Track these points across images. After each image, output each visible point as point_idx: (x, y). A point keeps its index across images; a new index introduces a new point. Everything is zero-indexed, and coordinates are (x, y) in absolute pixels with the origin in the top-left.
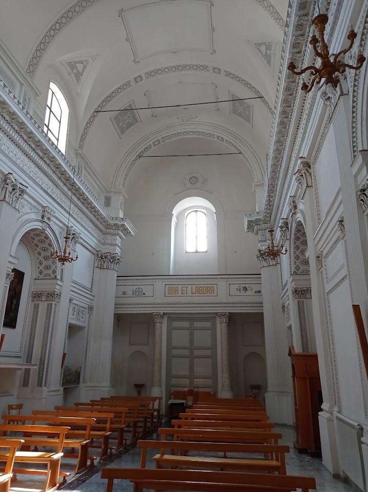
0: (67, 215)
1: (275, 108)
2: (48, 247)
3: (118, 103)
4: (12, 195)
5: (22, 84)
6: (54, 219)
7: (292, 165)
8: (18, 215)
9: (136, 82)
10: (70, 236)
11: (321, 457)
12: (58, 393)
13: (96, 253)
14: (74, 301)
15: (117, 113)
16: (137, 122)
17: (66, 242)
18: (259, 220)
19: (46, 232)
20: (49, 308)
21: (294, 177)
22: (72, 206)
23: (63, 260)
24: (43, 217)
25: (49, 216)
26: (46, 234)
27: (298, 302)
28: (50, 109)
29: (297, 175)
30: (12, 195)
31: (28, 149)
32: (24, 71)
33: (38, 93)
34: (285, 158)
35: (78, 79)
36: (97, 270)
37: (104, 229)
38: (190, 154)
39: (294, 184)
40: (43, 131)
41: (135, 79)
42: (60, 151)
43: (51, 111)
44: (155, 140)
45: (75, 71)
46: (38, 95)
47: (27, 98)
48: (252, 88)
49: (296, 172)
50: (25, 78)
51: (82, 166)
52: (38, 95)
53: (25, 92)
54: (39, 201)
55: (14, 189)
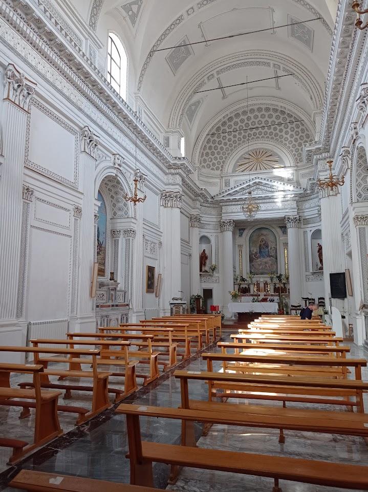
0: (134, 161)
1: (335, 28)
2: (116, 184)
3: (173, 40)
4: (90, 146)
5: (86, 39)
6: (123, 165)
7: (353, 91)
8: (97, 163)
9: (189, 15)
10: (139, 178)
11: (289, 297)
12: (140, 314)
13: (189, 216)
14: (146, 237)
15: (172, 51)
16: (190, 54)
17: (136, 184)
18: (319, 149)
19: (118, 178)
20: (128, 241)
21: (356, 103)
22: (137, 150)
23: (135, 200)
24: (115, 164)
25: (119, 162)
26: (118, 180)
27: (359, 228)
28: (111, 56)
29: (359, 101)
30: (18, 94)
31: (83, 86)
32: (87, 25)
33: (102, 46)
34: (338, 121)
35: (133, 22)
36: (162, 208)
37: (193, 197)
38: (230, 35)
39: (356, 111)
40: (105, 80)
41: (187, 11)
42: (120, 97)
43: (111, 58)
44: (209, 74)
45: (130, 13)
46: (101, 48)
47: (92, 52)
48: (311, 8)
49: (357, 99)
50: (89, 33)
51: (141, 110)
52: (101, 48)
53: (90, 47)
54: (68, 114)
55: (90, 141)
